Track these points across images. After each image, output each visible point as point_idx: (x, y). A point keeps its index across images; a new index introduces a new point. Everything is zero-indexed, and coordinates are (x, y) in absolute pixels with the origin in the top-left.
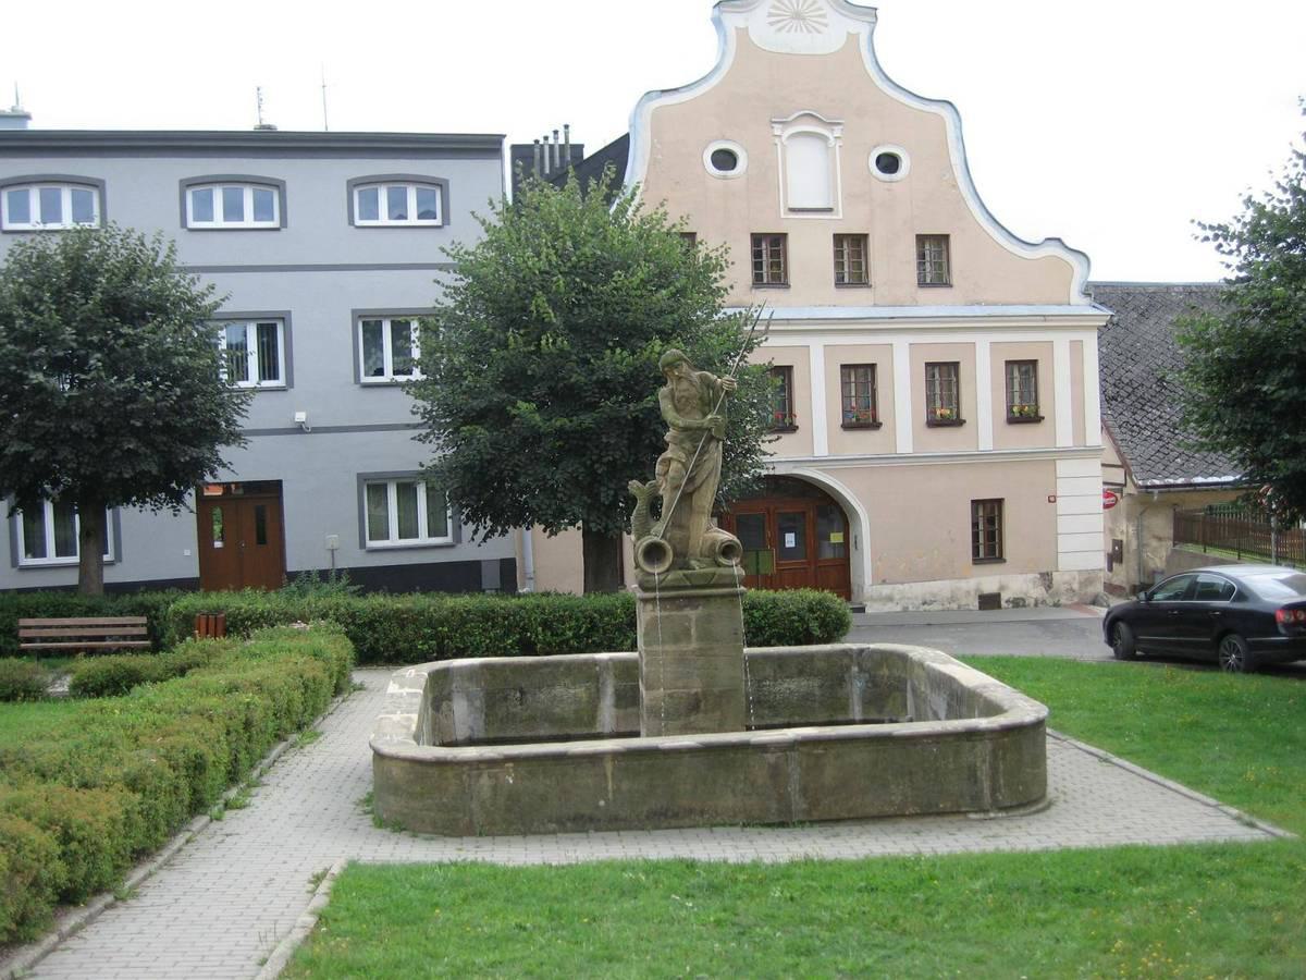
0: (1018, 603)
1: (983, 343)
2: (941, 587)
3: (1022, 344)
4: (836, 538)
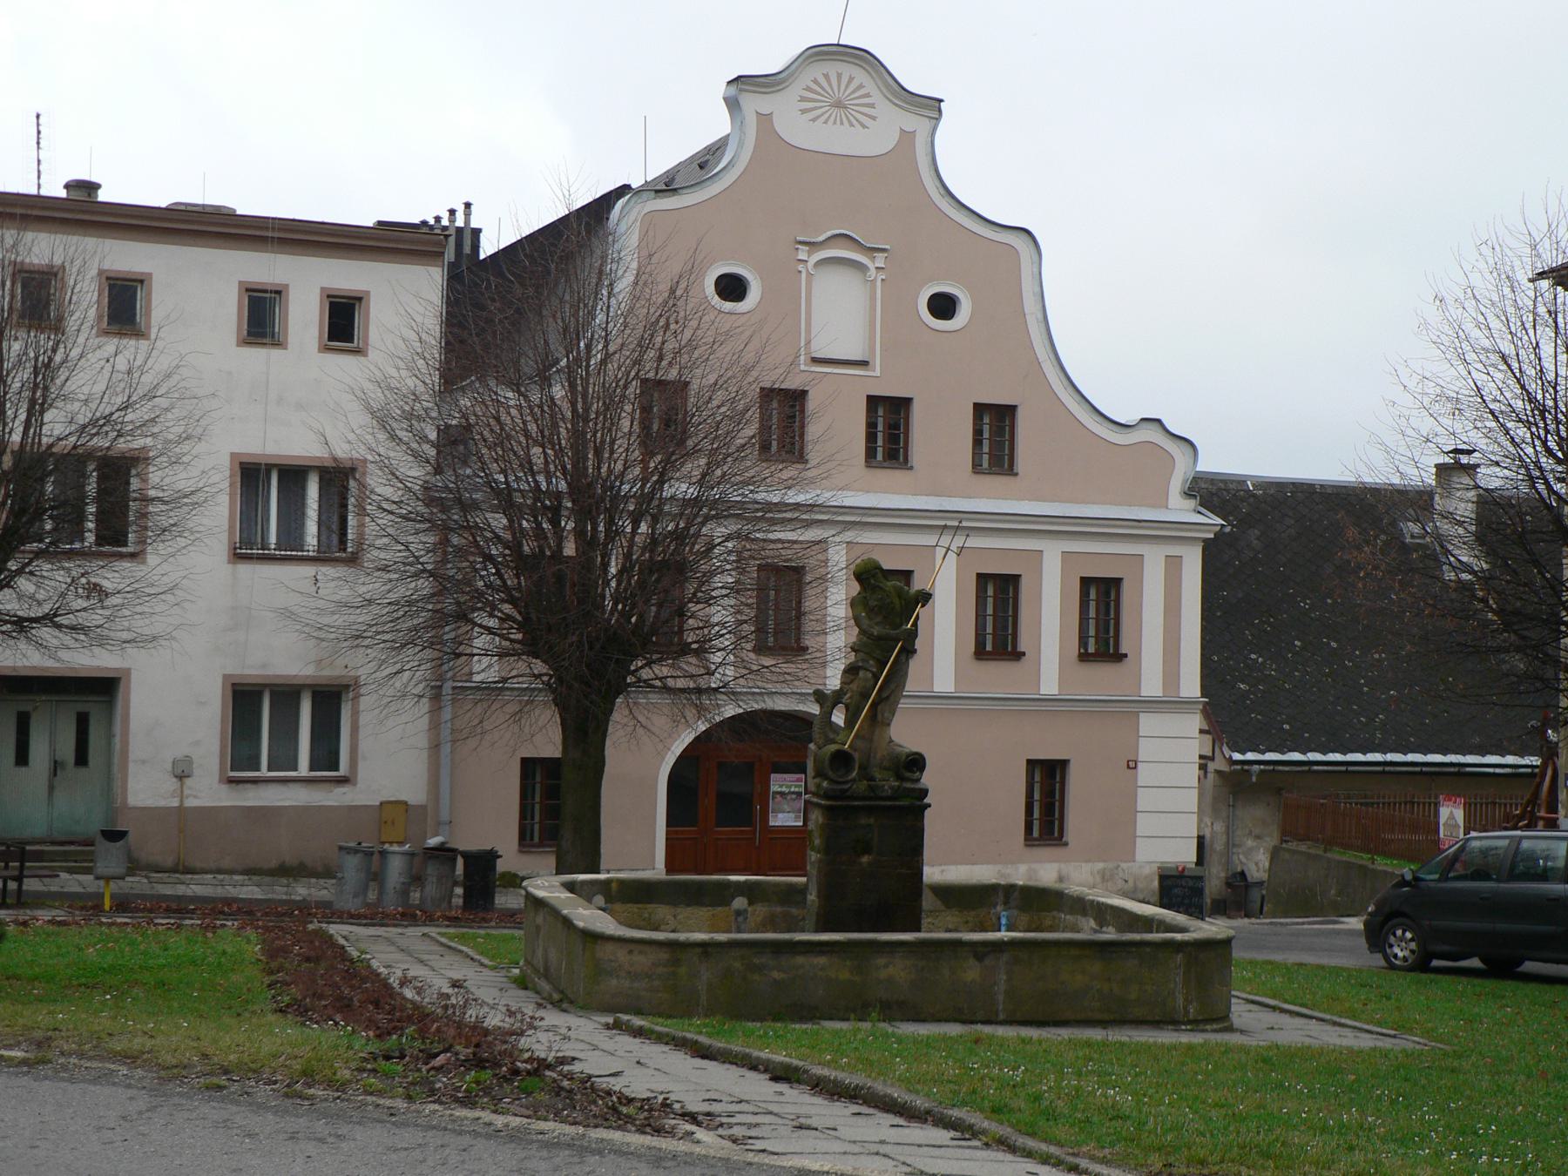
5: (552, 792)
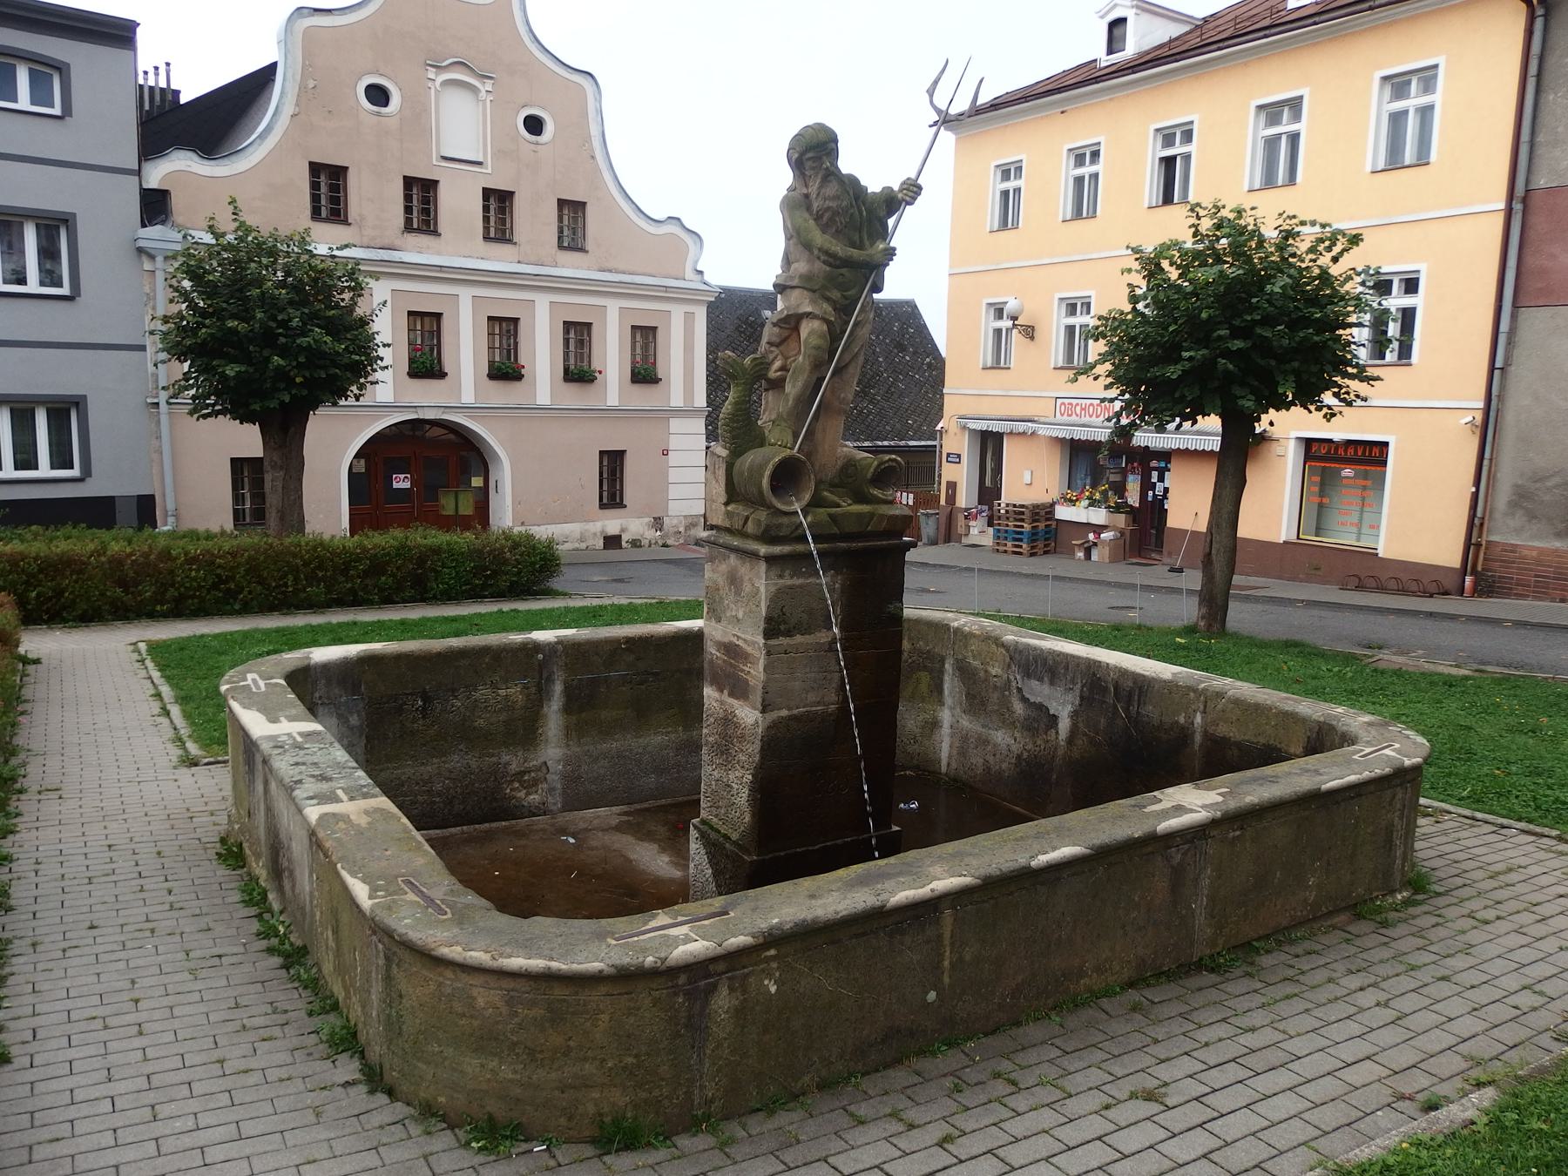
0: (635, 543)
1: (613, 307)
3: (645, 313)
4: (477, 482)
5: (258, 484)
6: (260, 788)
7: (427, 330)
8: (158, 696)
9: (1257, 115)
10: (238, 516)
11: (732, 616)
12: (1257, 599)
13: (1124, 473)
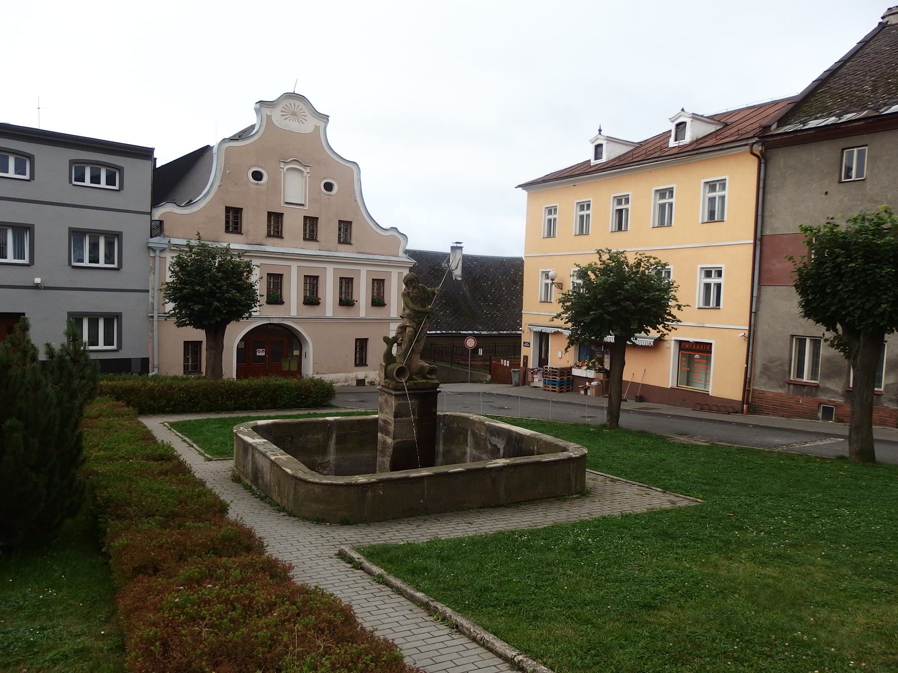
0: (372, 383)
1: (364, 270)
2: (341, 376)
4: (296, 353)
6: (250, 457)
7: (276, 281)
8: (185, 441)
9: (655, 194)
10: (186, 368)
11: (384, 411)
12: (652, 414)
13: (603, 354)
